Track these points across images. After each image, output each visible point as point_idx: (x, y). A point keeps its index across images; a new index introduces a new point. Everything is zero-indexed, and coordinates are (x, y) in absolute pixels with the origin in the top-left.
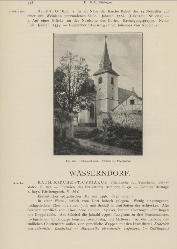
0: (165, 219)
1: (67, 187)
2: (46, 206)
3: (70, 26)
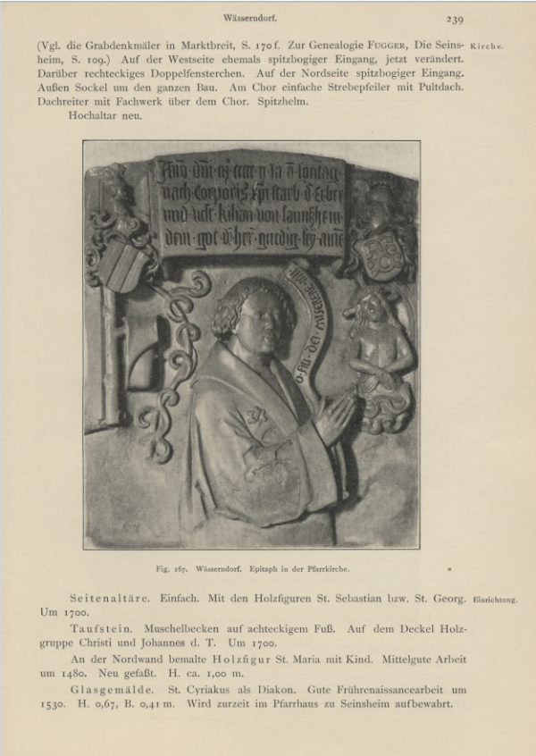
3: (311, 691)
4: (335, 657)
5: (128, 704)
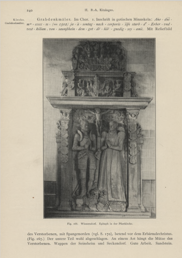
0: (169, 239)
1: (152, 234)
4: (62, 233)
5: (156, 29)
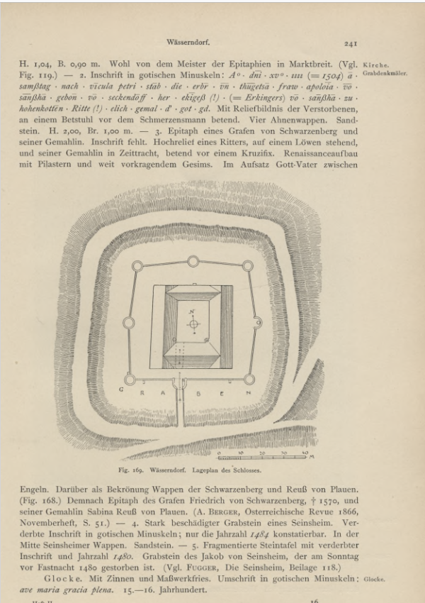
2: (309, 65)
